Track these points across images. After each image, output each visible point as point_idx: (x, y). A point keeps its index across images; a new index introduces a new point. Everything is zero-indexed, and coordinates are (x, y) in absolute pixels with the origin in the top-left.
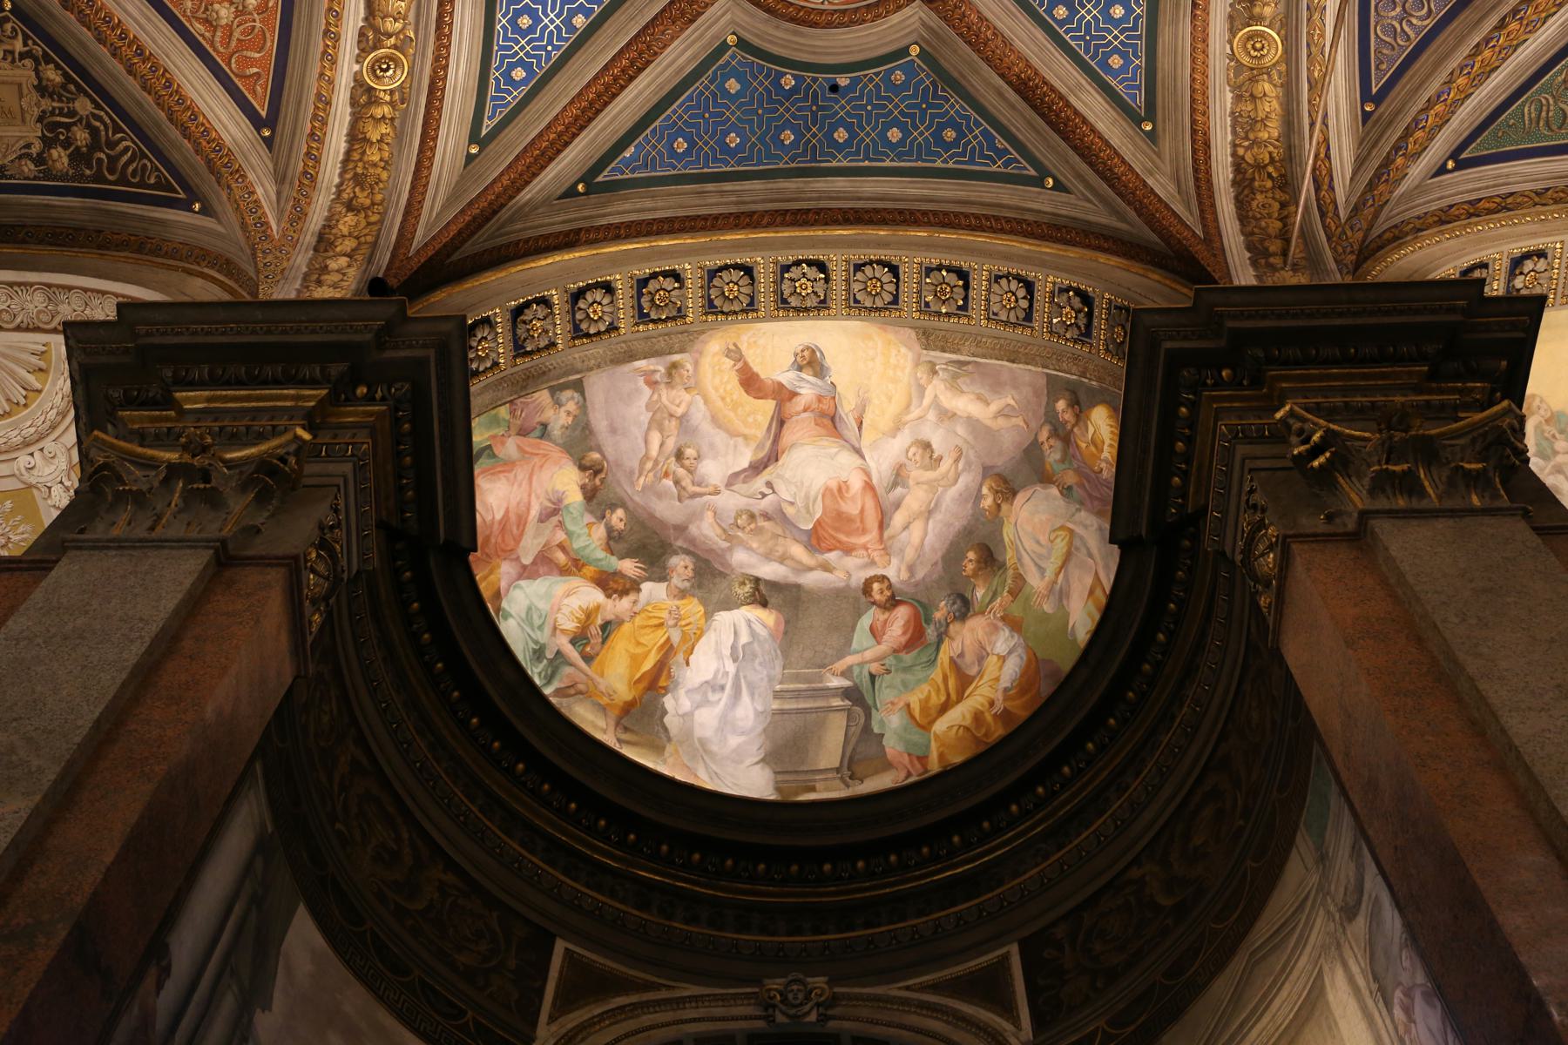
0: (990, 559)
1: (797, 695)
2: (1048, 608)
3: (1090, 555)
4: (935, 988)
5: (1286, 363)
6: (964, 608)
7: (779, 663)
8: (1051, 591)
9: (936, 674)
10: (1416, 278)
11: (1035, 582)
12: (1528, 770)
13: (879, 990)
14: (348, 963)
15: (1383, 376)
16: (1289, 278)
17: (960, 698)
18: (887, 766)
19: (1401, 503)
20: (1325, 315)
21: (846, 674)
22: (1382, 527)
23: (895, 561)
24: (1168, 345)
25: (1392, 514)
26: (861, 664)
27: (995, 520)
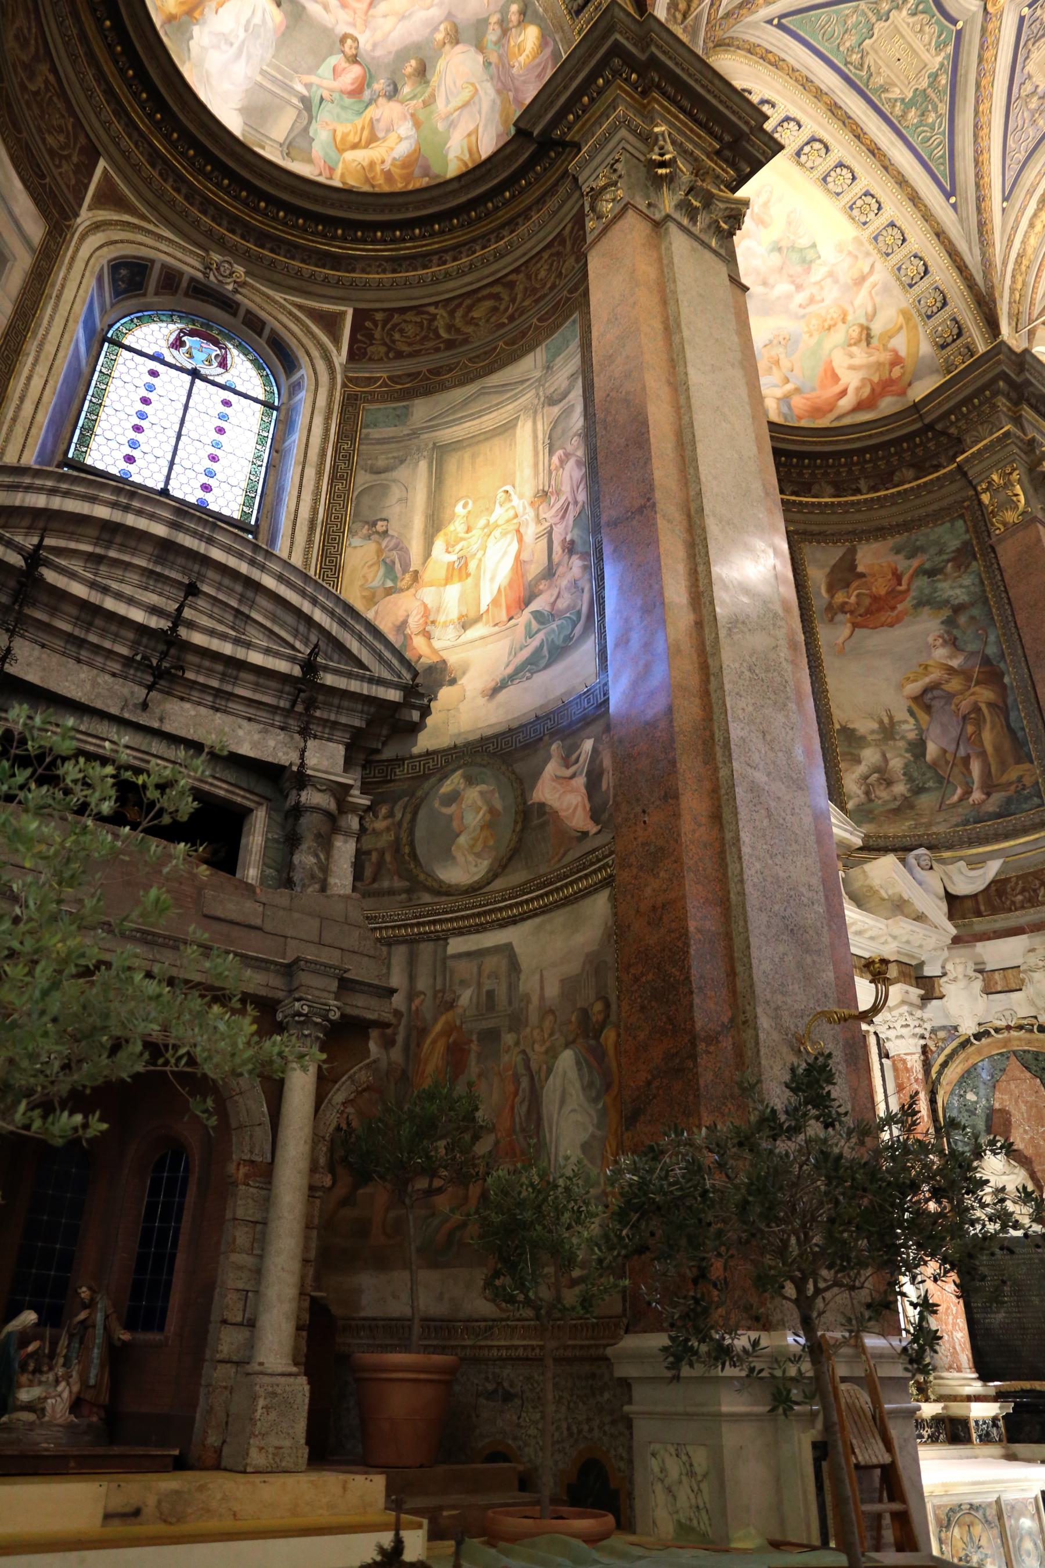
0: (422, 72)
1: (274, 80)
2: (441, 126)
3: (480, 112)
5: (664, 93)
6: (393, 92)
7: (271, 51)
8: (447, 117)
9: (359, 122)
10: (726, 77)
11: (441, 105)
12: (688, 398)
13: (270, 292)
15: (699, 137)
16: (678, 30)
17: (366, 146)
18: (310, 161)
19: (685, 222)
20: (696, 80)
21: (308, 86)
22: (673, 228)
23: (368, 33)
24: (618, 36)
25: (680, 226)
26: (319, 86)
27: (438, 53)
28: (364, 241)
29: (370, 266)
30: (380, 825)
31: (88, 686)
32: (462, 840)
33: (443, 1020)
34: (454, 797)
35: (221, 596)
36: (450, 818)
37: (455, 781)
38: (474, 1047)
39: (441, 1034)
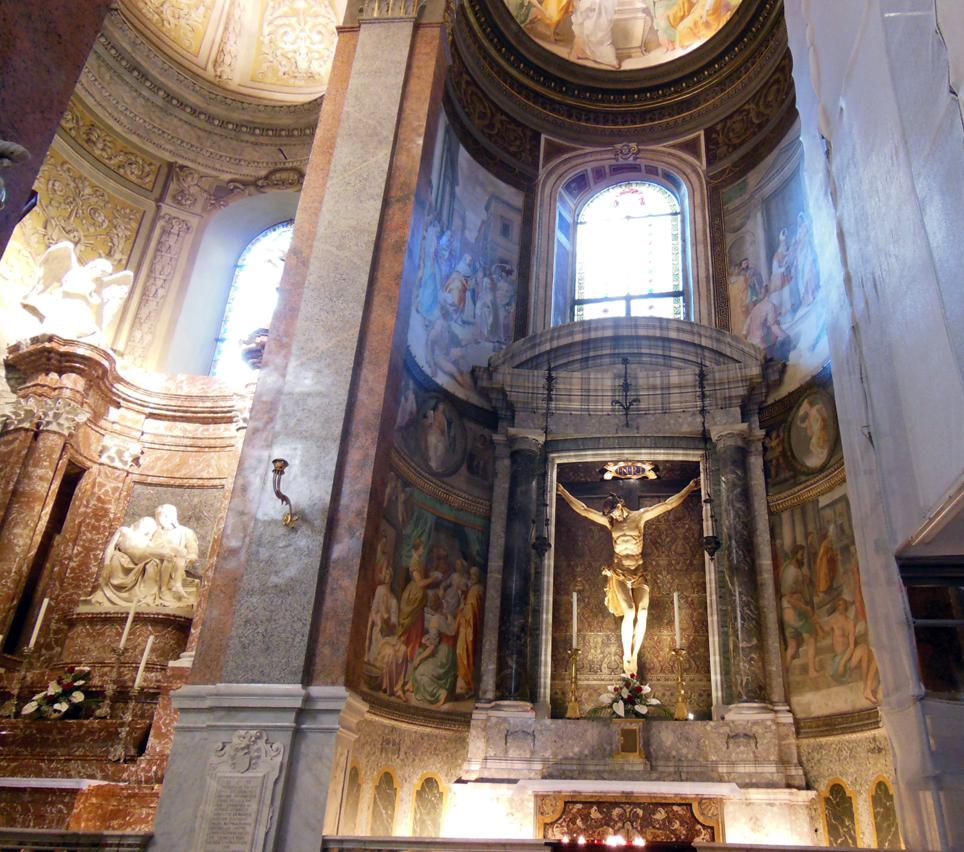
4: (674, 146)
14: (478, 161)
28: (699, 82)
29: (708, 95)
30: (774, 444)
31: (597, 425)
32: (814, 440)
33: (823, 544)
34: (806, 417)
35: (653, 352)
36: (806, 429)
37: (805, 407)
38: (839, 557)
39: (823, 555)
